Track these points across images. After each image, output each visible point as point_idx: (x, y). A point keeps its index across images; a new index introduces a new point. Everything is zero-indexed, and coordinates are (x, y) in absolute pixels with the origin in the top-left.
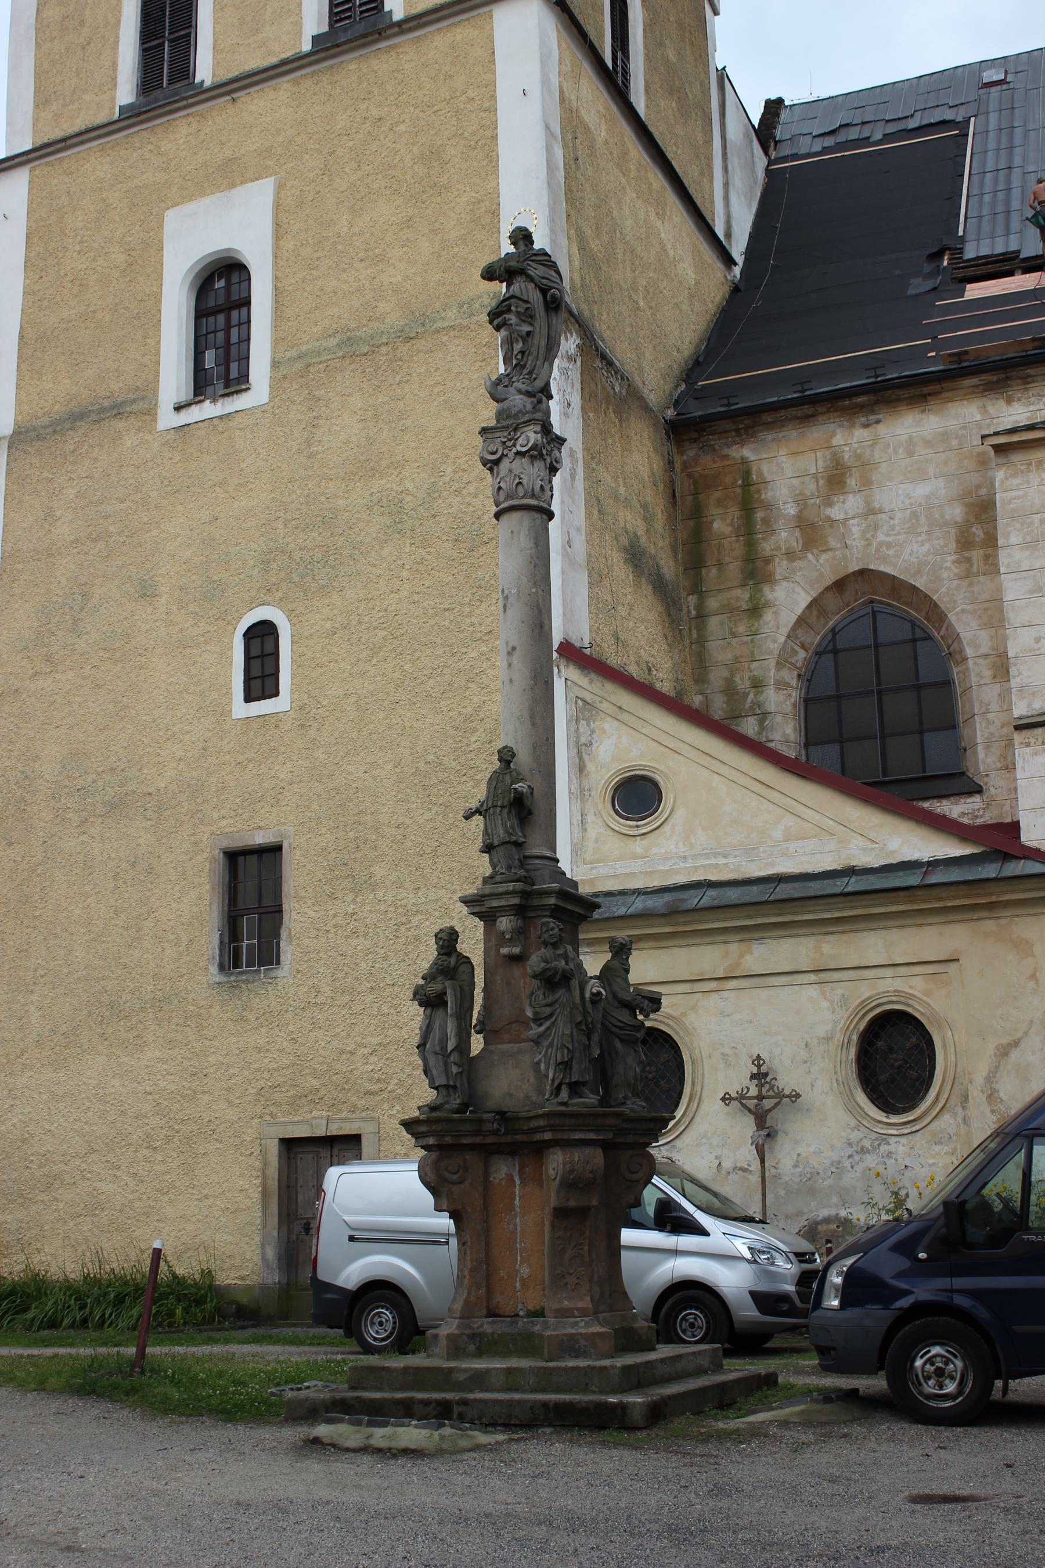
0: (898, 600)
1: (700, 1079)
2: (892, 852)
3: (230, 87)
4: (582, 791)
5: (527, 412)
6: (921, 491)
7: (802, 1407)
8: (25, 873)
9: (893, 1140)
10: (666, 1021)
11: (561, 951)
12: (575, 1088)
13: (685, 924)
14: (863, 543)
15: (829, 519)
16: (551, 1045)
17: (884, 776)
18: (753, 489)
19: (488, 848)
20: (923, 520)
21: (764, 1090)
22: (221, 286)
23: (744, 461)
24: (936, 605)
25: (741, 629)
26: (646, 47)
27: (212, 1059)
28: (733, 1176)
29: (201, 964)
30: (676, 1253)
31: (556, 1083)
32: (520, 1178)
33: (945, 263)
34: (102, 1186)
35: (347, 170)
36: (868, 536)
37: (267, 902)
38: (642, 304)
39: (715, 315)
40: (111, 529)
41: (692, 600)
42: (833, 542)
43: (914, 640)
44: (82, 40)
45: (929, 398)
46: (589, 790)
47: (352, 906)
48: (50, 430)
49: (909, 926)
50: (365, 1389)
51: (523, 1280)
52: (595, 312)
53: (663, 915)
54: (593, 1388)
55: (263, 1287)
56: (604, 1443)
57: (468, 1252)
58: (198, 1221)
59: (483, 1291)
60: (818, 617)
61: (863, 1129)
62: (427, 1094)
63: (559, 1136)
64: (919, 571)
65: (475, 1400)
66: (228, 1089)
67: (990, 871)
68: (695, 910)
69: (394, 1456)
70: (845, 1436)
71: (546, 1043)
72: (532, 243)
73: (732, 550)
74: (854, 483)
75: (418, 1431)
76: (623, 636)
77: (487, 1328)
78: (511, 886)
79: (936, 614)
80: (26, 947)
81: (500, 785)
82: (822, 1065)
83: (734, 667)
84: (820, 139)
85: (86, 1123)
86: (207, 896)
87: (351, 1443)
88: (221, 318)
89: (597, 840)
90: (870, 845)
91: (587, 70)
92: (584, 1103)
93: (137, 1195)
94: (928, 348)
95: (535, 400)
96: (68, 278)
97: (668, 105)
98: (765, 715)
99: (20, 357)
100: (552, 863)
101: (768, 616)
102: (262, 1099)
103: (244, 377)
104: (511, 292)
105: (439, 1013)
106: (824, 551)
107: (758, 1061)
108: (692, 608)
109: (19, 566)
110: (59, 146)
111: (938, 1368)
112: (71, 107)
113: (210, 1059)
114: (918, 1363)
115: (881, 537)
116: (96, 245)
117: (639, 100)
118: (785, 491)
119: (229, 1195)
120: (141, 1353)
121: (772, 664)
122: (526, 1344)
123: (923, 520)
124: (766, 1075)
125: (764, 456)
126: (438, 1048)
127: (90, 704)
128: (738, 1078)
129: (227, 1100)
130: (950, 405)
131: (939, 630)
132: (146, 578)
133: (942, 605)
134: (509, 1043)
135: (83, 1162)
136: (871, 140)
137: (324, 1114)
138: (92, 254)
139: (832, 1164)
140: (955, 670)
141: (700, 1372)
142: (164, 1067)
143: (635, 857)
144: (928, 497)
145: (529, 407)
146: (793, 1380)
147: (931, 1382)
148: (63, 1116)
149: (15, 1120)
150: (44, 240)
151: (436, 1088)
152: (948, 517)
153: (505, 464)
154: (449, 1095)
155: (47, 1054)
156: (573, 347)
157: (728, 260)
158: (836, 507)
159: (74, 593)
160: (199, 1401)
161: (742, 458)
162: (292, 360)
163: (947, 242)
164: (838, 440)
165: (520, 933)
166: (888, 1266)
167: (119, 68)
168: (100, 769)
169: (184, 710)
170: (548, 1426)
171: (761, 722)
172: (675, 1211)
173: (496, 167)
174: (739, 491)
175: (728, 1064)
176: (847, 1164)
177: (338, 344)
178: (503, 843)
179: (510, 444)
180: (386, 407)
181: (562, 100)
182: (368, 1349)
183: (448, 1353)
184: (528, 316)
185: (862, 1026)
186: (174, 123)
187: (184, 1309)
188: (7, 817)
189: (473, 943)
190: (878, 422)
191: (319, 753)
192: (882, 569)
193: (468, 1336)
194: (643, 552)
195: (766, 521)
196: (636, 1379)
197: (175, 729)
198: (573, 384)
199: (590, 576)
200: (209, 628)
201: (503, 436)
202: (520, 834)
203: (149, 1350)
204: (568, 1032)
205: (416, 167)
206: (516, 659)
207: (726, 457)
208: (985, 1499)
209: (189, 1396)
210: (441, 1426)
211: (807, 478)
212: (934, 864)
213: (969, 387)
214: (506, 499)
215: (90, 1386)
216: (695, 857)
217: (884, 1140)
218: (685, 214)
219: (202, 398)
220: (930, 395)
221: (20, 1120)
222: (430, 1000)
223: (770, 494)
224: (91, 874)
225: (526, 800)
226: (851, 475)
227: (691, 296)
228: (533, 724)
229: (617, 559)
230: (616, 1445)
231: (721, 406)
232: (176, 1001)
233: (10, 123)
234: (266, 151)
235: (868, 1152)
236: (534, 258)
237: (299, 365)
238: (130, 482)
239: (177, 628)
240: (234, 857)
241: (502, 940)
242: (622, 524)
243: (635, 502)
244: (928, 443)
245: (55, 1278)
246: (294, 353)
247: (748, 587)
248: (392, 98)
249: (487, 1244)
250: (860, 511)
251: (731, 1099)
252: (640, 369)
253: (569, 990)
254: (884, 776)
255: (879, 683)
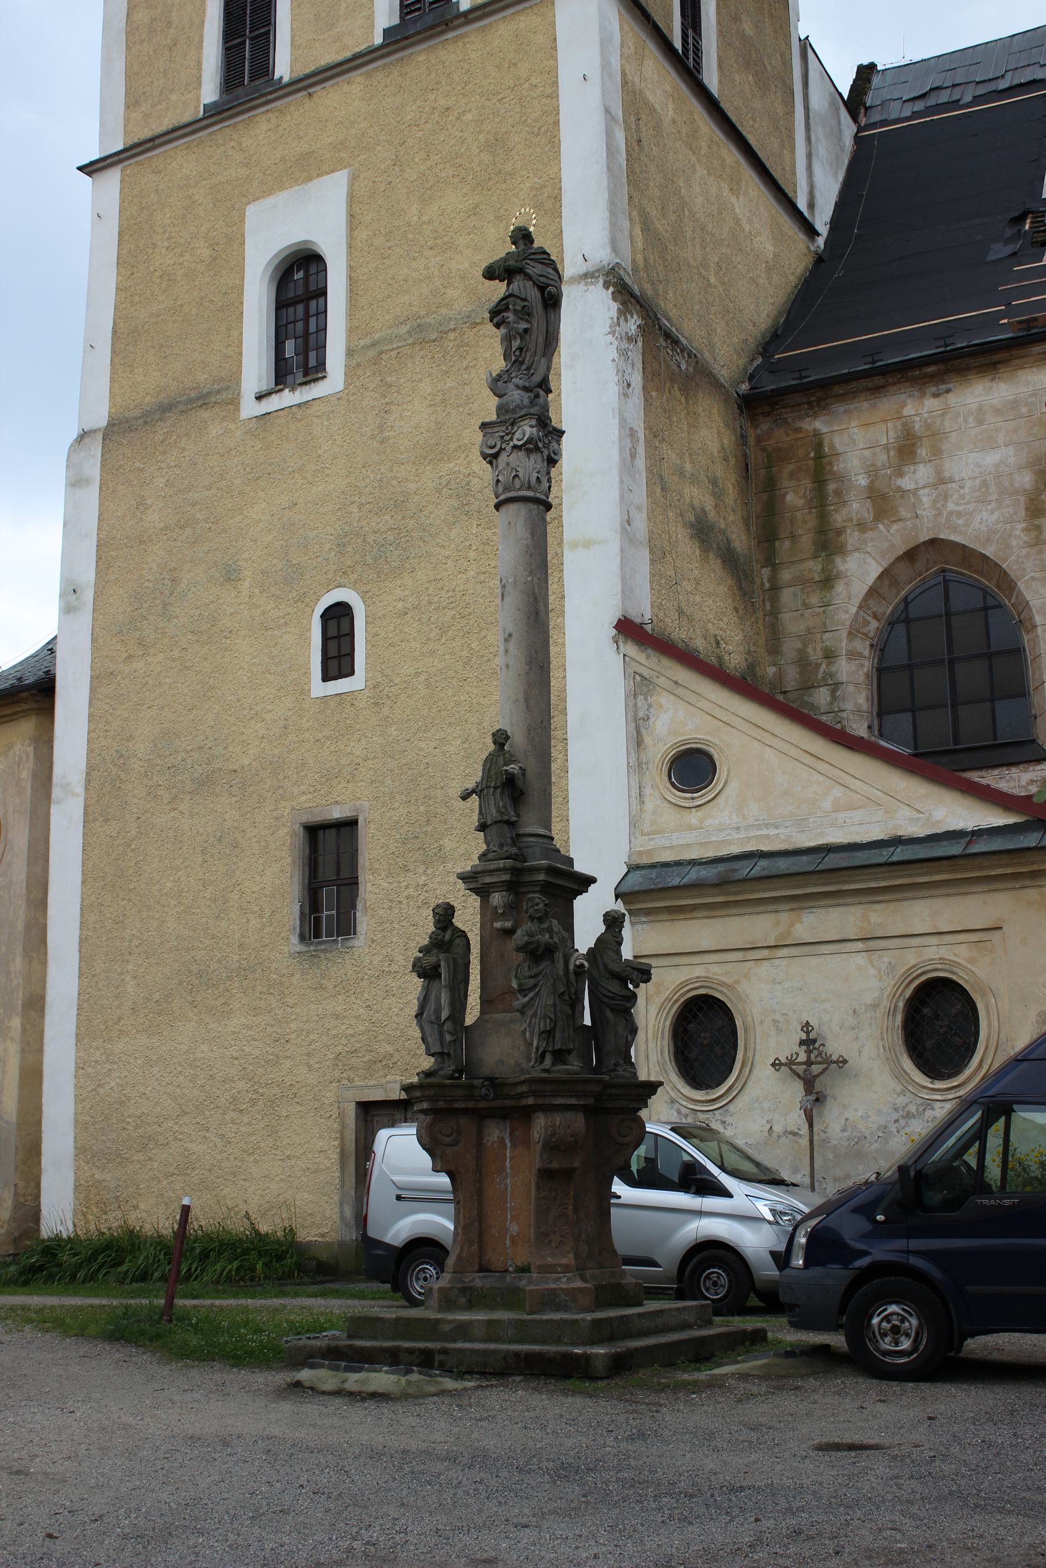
0: (969, 568)
1: (752, 1045)
2: (937, 822)
3: (308, 82)
4: (640, 764)
5: (525, 407)
6: (991, 459)
7: (765, 1361)
8: (121, 848)
9: (938, 1105)
10: (720, 988)
11: (545, 926)
12: (560, 1056)
13: (737, 893)
14: (934, 512)
15: (899, 489)
16: (535, 1015)
17: (955, 744)
18: (824, 461)
19: (482, 827)
20: (993, 489)
21: (813, 1056)
22: (299, 279)
23: (817, 434)
24: (1006, 573)
25: (814, 600)
26: (719, 23)
27: (293, 1026)
28: (783, 1140)
29: (283, 934)
30: (700, 1213)
31: (540, 1051)
32: (511, 1141)
33: (1027, 227)
34: (193, 1147)
35: (417, 160)
36: (938, 505)
37: (345, 874)
38: (713, 280)
39: (796, 286)
40: (198, 516)
41: (766, 572)
42: (904, 513)
43: (986, 609)
44: (169, 41)
45: (998, 366)
46: (647, 763)
47: (423, 878)
48: (141, 421)
49: (954, 895)
50: (361, 1338)
51: (512, 1237)
52: (660, 292)
53: (716, 885)
54: (565, 1339)
55: (341, 1244)
56: (565, 1392)
57: (462, 1211)
58: (282, 1180)
59: (475, 1248)
60: (890, 587)
61: (908, 1094)
62: (427, 1063)
63: (540, 1101)
64: (988, 540)
65: (454, 1349)
66: (309, 1055)
67: (1031, 840)
68: (744, 880)
69: (364, 1399)
70: (797, 1388)
71: (530, 1013)
72: (532, 242)
73: (805, 522)
74: (924, 454)
75: (387, 1376)
76: (688, 611)
77: (478, 1283)
78: (501, 864)
79: (1007, 583)
80: (122, 918)
81: (493, 767)
82: (869, 1032)
83: (806, 639)
84: (911, 103)
85: (178, 1086)
86: (289, 869)
87: (328, 1387)
88: (300, 308)
89: (654, 813)
90: (916, 815)
91: (652, 49)
92: (566, 1070)
93: (225, 1155)
94: (1001, 315)
95: (532, 395)
96: (157, 274)
97: (744, 80)
98: (837, 685)
99: (113, 351)
100: (549, 841)
101: (840, 587)
102: (340, 1064)
103: (321, 365)
104: (510, 291)
105: (435, 984)
106: (895, 521)
107: (807, 1027)
108: (765, 580)
109: (114, 554)
110: (148, 146)
111: (894, 1326)
112: (158, 107)
113: (291, 1025)
114: (875, 1321)
115: (951, 506)
116: (182, 241)
117: (711, 79)
118: (856, 462)
119: (310, 1156)
120: (170, 1304)
121: (844, 634)
122: (511, 1298)
123: (993, 489)
124: (814, 1041)
125: (837, 428)
126: (433, 1018)
127: (179, 685)
128: (788, 1046)
129: (308, 1064)
130: (1020, 372)
131: (1009, 598)
132: (230, 562)
133: (1011, 574)
134: (503, 1012)
135: (176, 1123)
136: (961, 103)
137: (398, 1078)
138: (179, 250)
139: (879, 1129)
140: (1026, 638)
141: (686, 1326)
142: (250, 1033)
143: (690, 828)
144: (997, 465)
145: (526, 402)
146: (780, 1336)
147: (887, 1339)
148: (157, 1080)
149: (113, 1084)
150: (135, 240)
151: (432, 1055)
152: (1017, 485)
153: (503, 458)
154: (443, 1062)
155: (142, 1021)
156: (634, 328)
157: (811, 232)
158: (907, 478)
159: (164, 579)
160: (215, 1347)
161: (815, 430)
162: (367, 348)
163: (1030, 205)
164: (908, 410)
165: (512, 908)
166: (850, 1228)
167: (204, 67)
168: (189, 748)
169: (266, 690)
170: (520, 1374)
171: (833, 692)
172: (701, 1173)
173: (558, 153)
174: (811, 463)
175: (779, 1031)
176: (893, 1128)
177: (408, 332)
178: (496, 822)
179: (507, 438)
180: (454, 392)
181: (625, 82)
182: (414, 1303)
183: (439, 1306)
184: (525, 313)
185: (908, 994)
186: (254, 120)
187: (265, 1265)
188: (104, 795)
189: (468, 917)
190: (948, 391)
191: (393, 731)
192: (952, 538)
193: (459, 1289)
194: (712, 527)
195: (838, 493)
196: (602, 1332)
197: (258, 708)
198: (633, 365)
199: (651, 552)
200: (289, 610)
201: (500, 431)
202: (512, 813)
203: (179, 1302)
204: (550, 1002)
205: (482, 154)
206: (512, 646)
207: (799, 430)
208: (888, 1448)
209: (207, 1342)
210: (409, 1372)
211: (878, 449)
212: (978, 834)
213: (1039, 354)
214: (503, 492)
215: (123, 1333)
216: (748, 828)
217: (929, 1105)
218: (762, 188)
219: (281, 387)
220: (999, 362)
221: (118, 1084)
222: (427, 972)
223: (841, 466)
224: (181, 848)
225: (517, 781)
226: (921, 445)
227: (769, 270)
228: (528, 707)
229: (682, 536)
230: (574, 1392)
231: (794, 379)
232: (260, 971)
233: (102, 125)
234: (341, 144)
235: (914, 1117)
236: (532, 257)
237: (372, 353)
238: (216, 470)
239: (259, 611)
240: (314, 832)
241: (496, 917)
242: (688, 500)
243: (703, 477)
244: (998, 412)
245: (149, 1234)
246: (367, 341)
247: (820, 559)
248: (459, 87)
249: (480, 1203)
250: (930, 481)
251: (781, 1064)
252: (711, 346)
253: (553, 962)
254: (955, 744)
255: (950, 651)
